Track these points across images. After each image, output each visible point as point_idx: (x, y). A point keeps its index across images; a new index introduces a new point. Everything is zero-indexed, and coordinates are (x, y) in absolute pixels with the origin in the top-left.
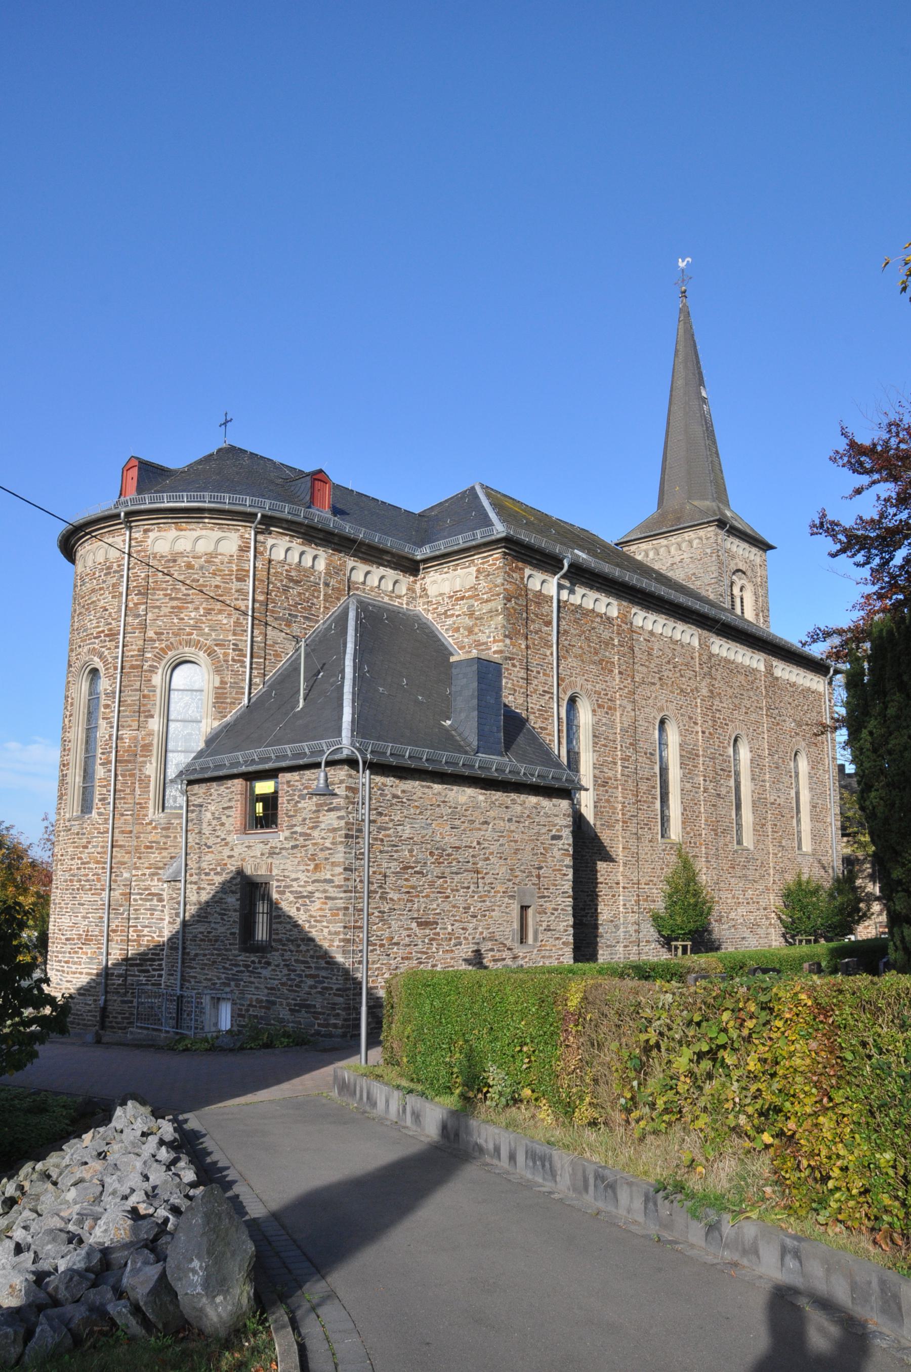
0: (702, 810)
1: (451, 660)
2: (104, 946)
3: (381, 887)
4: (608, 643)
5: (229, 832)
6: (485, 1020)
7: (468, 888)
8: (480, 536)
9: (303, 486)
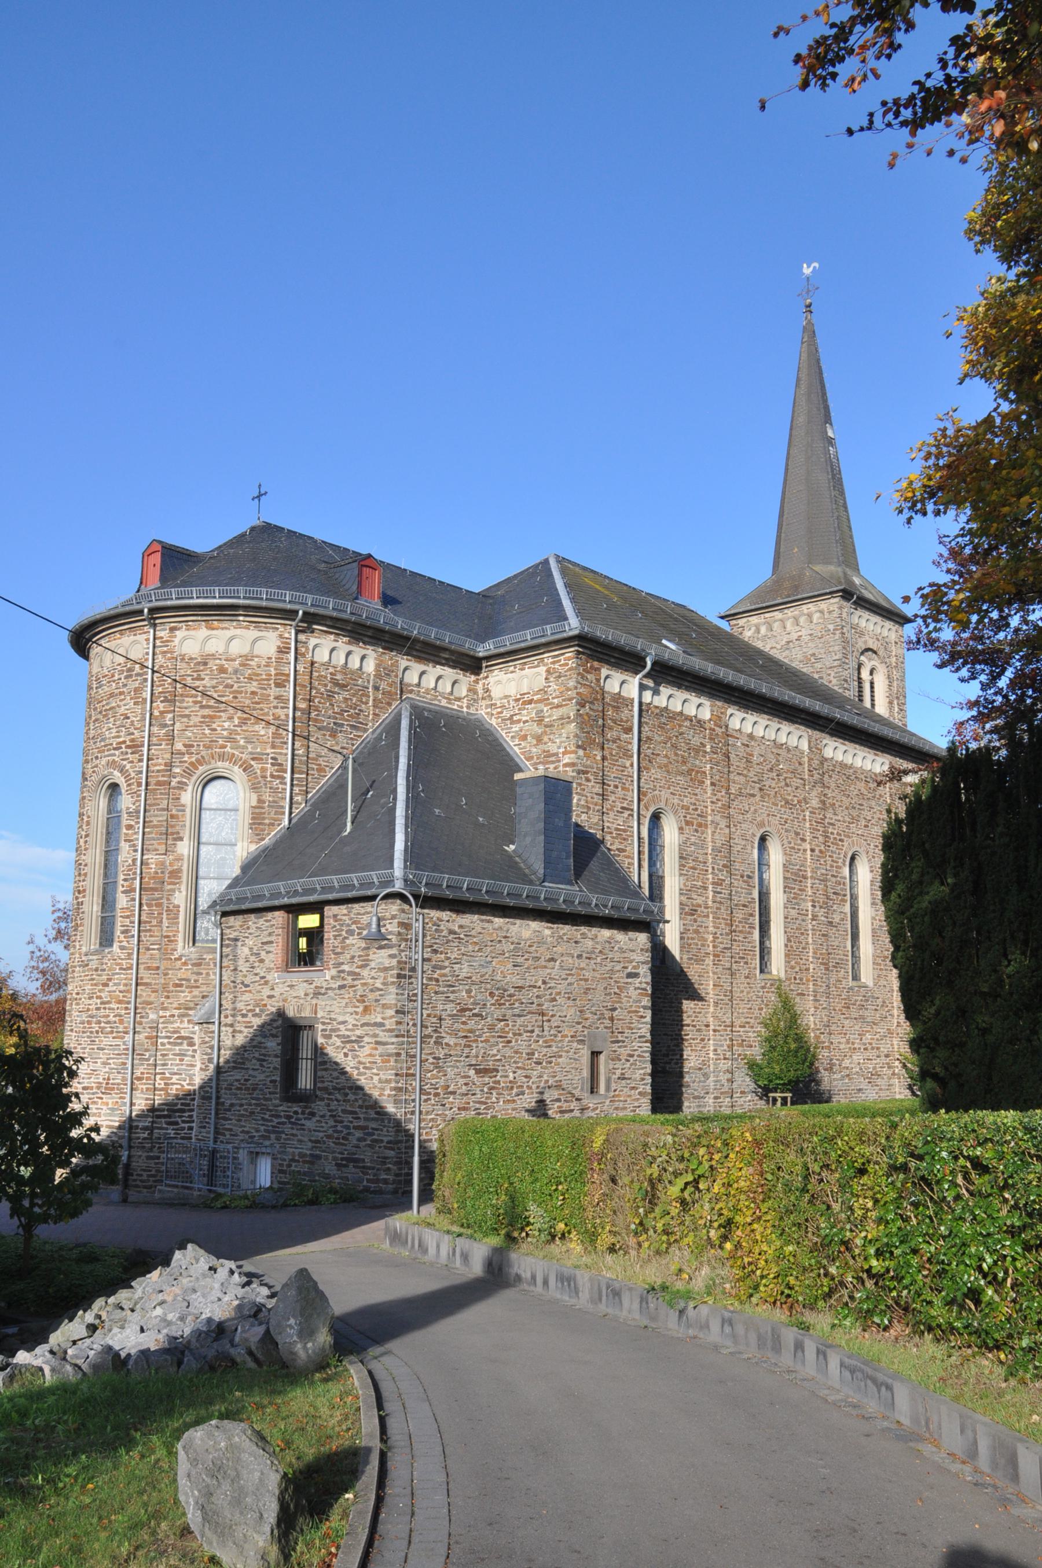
0: (810, 940)
1: (515, 778)
2: (128, 1096)
3: (435, 1031)
4: (699, 750)
5: (269, 970)
6: (527, 1163)
7: (532, 1031)
8: (550, 632)
9: (349, 573)
